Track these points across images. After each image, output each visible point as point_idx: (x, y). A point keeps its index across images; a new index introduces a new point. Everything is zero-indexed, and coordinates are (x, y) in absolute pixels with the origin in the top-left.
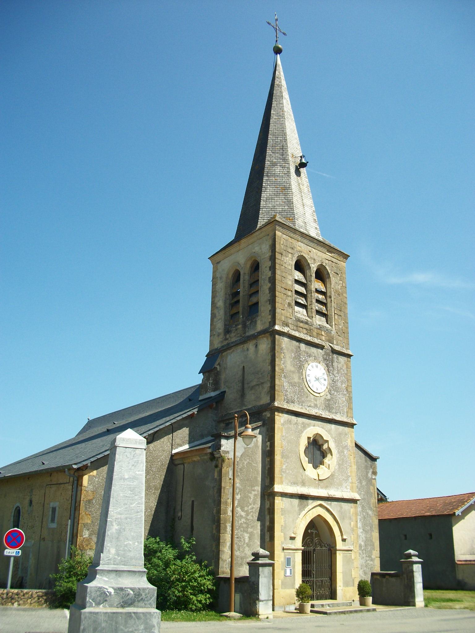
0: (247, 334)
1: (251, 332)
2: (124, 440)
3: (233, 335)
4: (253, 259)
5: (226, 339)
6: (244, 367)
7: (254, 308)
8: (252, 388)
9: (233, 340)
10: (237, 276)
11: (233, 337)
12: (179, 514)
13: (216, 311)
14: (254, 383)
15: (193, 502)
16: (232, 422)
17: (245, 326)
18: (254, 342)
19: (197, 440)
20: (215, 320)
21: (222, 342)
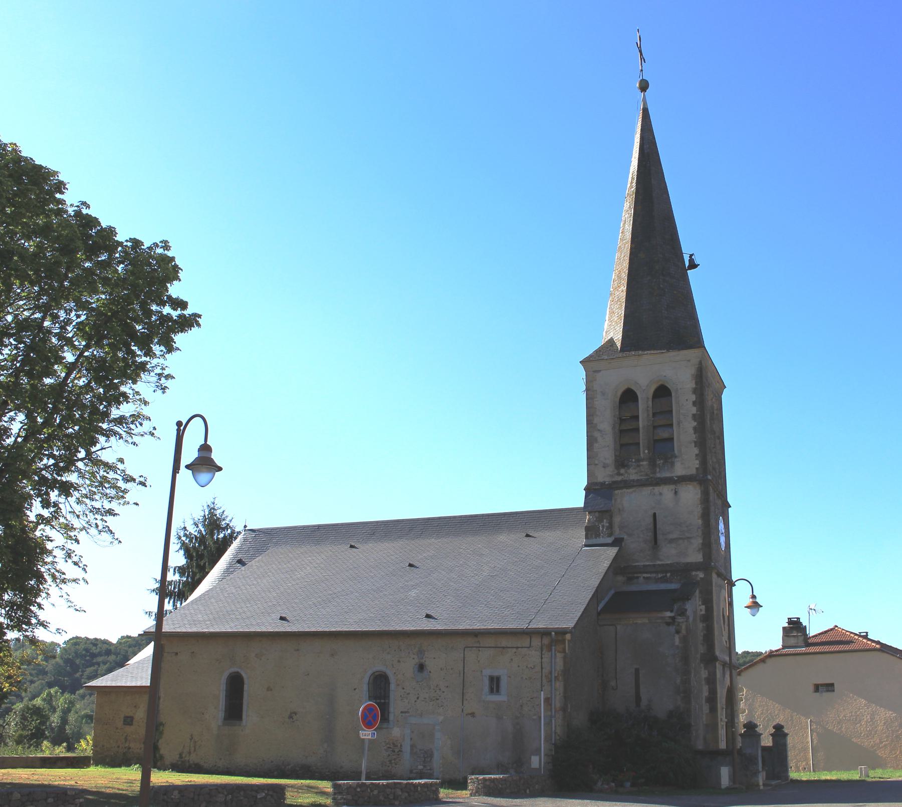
0: (658, 475)
1: (666, 474)
2: (75, 668)
3: (631, 471)
4: (660, 383)
5: (619, 474)
6: (655, 514)
7: (663, 449)
8: (671, 541)
9: (633, 477)
10: (629, 397)
11: (633, 474)
12: (613, 683)
13: (597, 434)
14: (674, 536)
15: (637, 670)
16: (638, 578)
17: (653, 464)
18: (673, 487)
19: (204, 595)
20: (596, 445)
21: (611, 476)
